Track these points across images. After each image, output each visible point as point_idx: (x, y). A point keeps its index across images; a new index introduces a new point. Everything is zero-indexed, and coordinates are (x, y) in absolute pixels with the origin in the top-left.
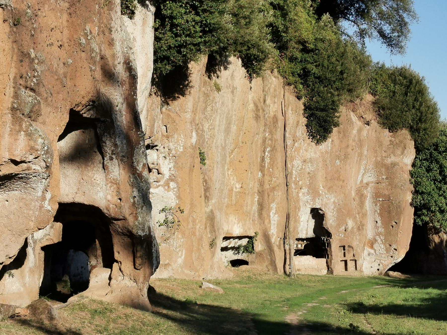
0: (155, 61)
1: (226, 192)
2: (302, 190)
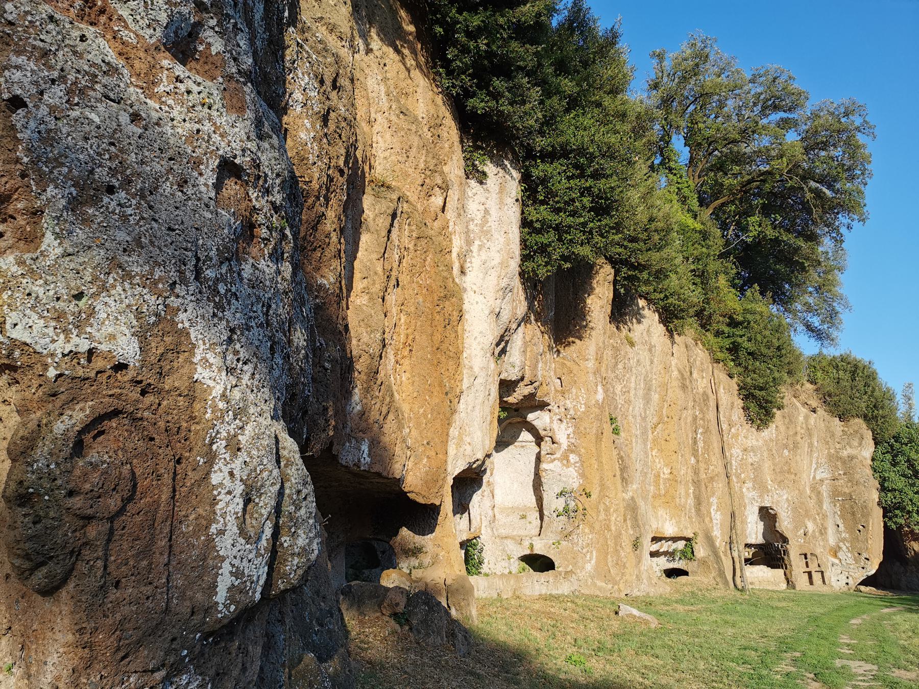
0: (525, 258)
1: (651, 477)
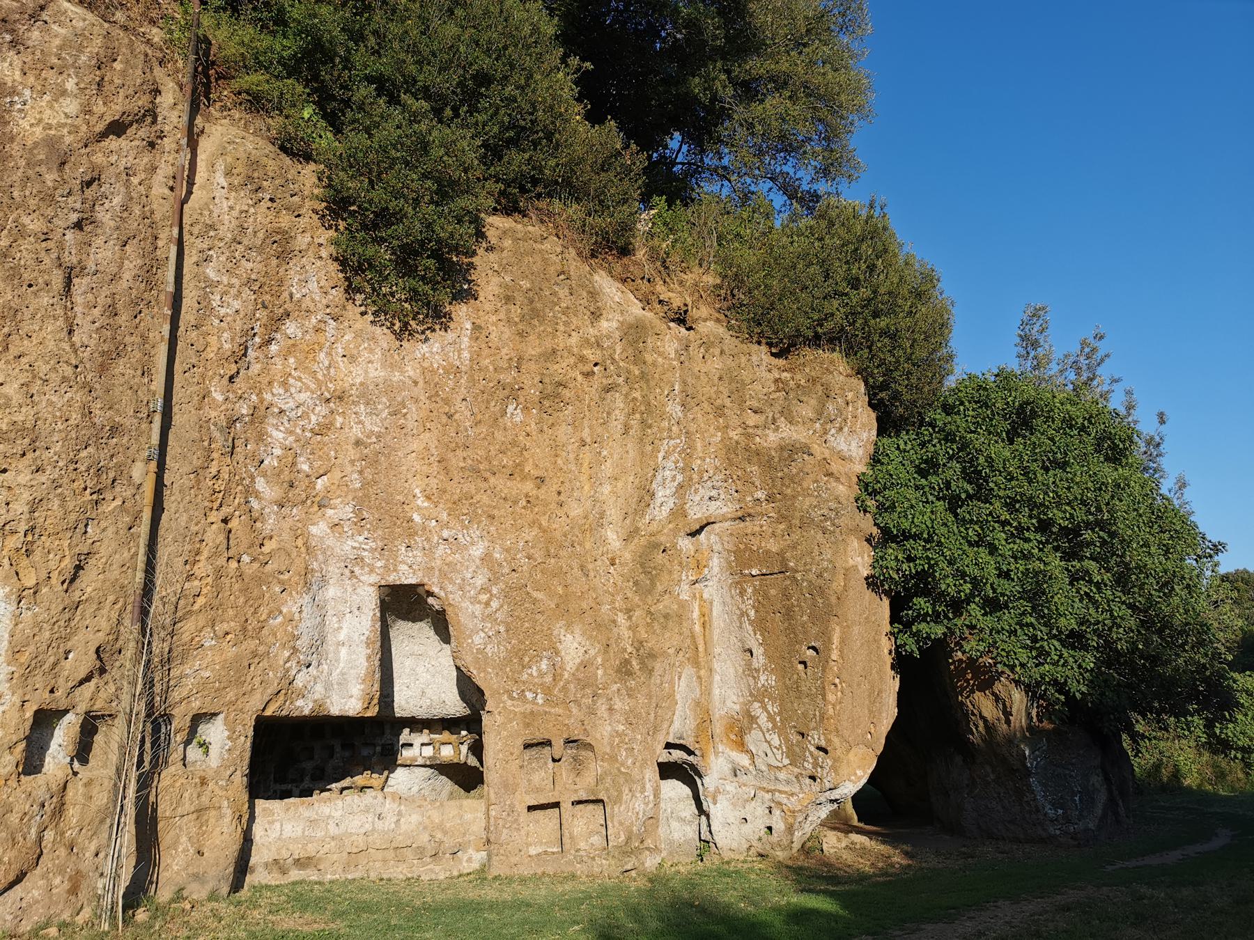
2: (330, 512)
